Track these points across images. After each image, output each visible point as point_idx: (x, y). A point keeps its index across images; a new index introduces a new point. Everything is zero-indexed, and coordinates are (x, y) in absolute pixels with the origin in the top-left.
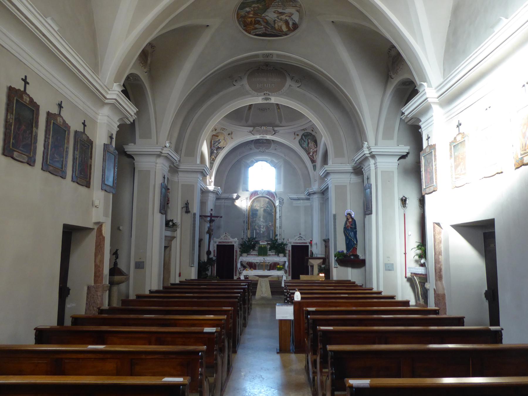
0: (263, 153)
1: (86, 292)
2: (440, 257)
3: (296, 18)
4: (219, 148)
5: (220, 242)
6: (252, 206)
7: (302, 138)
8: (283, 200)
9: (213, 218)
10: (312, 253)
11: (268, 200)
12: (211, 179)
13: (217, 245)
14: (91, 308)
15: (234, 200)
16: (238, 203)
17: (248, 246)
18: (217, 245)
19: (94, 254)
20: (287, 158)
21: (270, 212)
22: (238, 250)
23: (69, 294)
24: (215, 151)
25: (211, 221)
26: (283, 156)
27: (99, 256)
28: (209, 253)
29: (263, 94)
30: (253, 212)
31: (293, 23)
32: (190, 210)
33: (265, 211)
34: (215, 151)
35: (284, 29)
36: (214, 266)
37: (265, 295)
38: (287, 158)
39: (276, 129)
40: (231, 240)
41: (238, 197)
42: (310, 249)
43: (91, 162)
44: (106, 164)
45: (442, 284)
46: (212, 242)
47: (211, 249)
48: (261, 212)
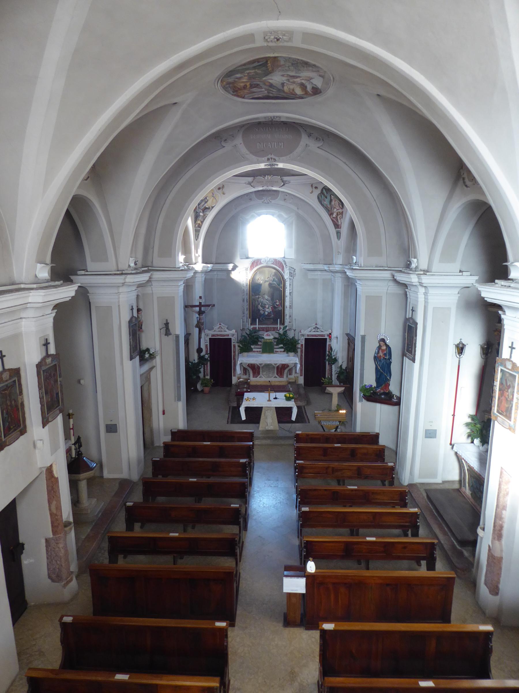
0: (267, 205)
1: (44, 544)
2: (504, 512)
3: (318, 82)
4: (205, 209)
5: (213, 335)
6: (253, 279)
7: (322, 192)
8: (294, 271)
9: (203, 309)
10: (331, 349)
11: (274, 271)
12: (197, 252)
13: (210, 339)
14: (54, 562)
15: (229, 272)
16: (234, 275)
18: (210, 339)
19: (47, 501)
20: (300, 212)
21: (278, 290)
23: (23, 549)
24: (201, 214)
26: (295, 208)
27: (54, 503)
28: (199, 350)
29: (266, 158)
30: (255, 288)
31: (313, 88)
32: (171, 331)
33: (270, 285)
34: (201, 214)
35: (299, 91)
36: (207, 364)
37: (271, 428)
38: (300, 212)
39: (285, 178)
40: (228, 332)
42: (328, 343)
43: (22, 399)
45: (501, 545)
46: (203, 335)
47: (203, 346)
48: (265, 287)
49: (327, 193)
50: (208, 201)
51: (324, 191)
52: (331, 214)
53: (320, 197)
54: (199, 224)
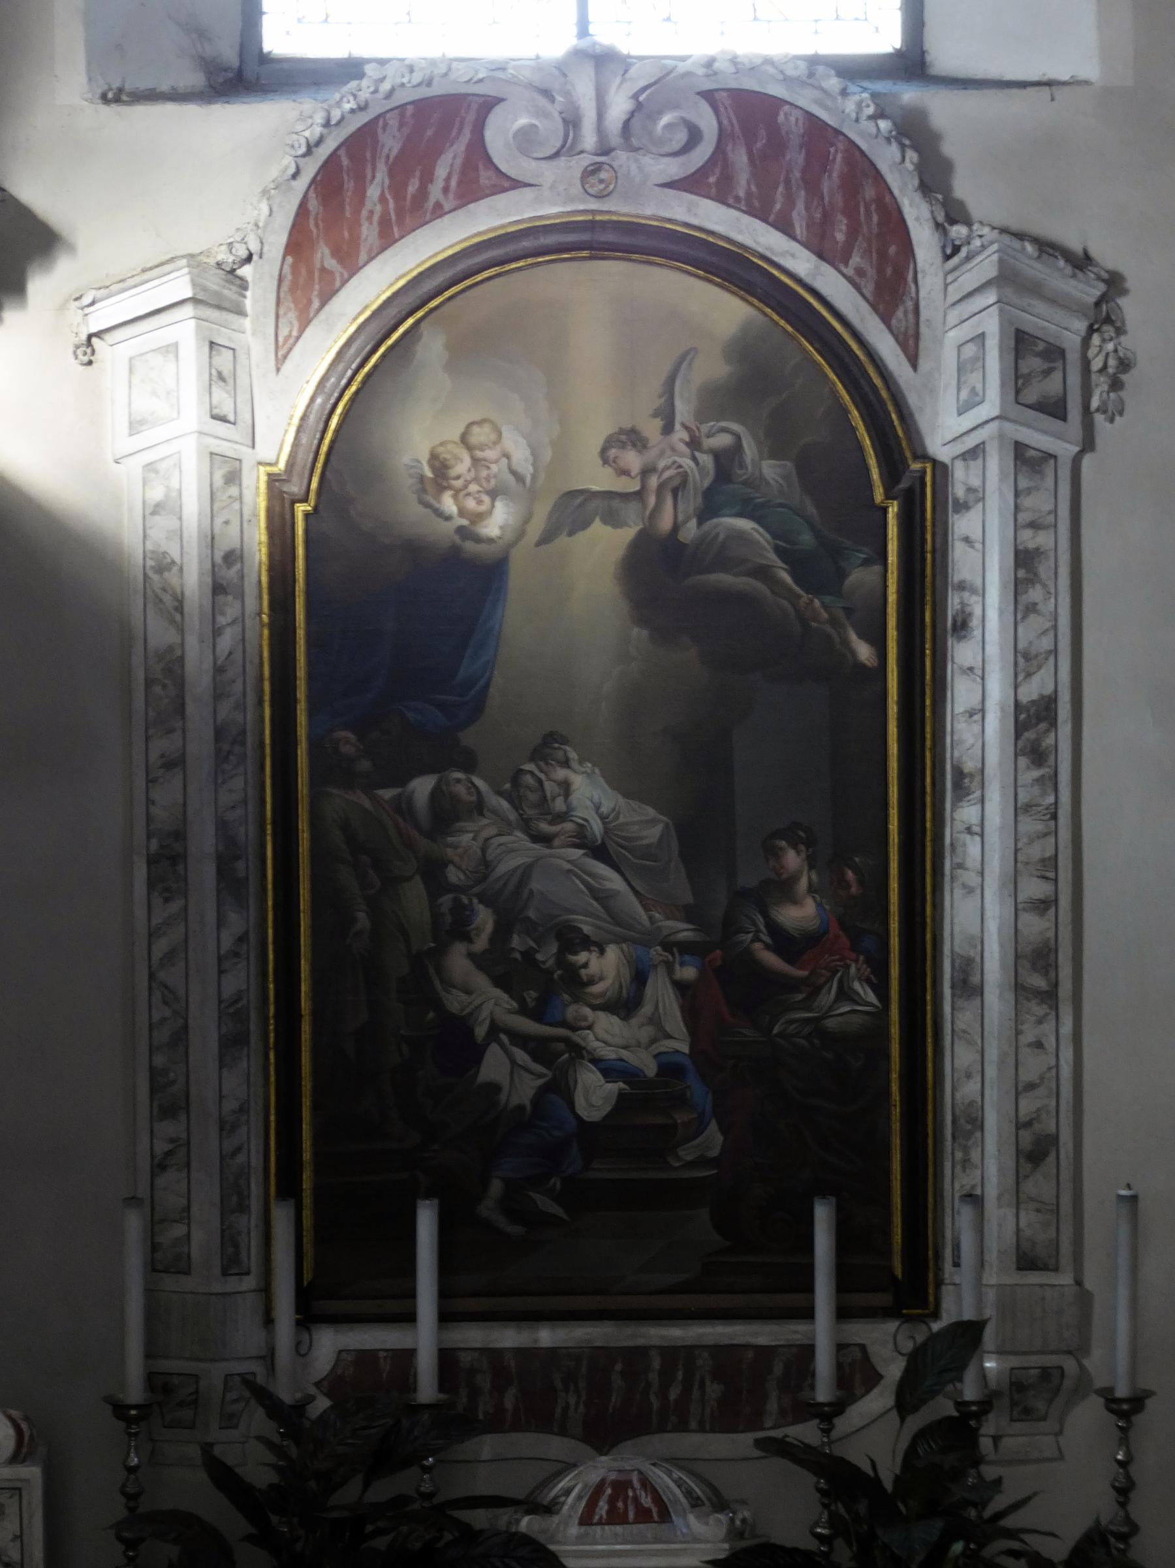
6: (344, 452)
8: (1104, 317)
11: (727, 312)
33: (660, 573)
44: (709, 1546)
48: (572, 608)
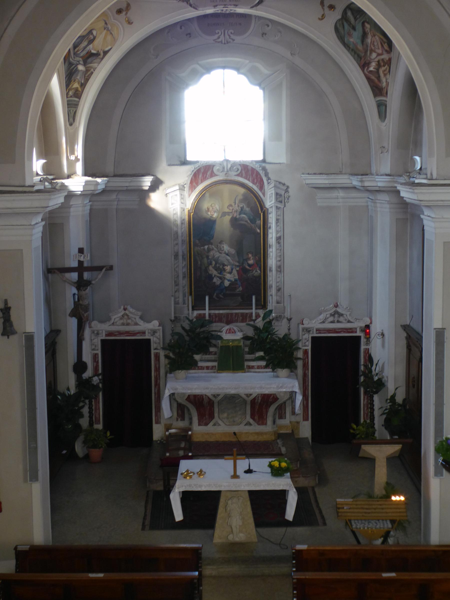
5: (110, 334)
6: (197, 208)
7: (344, 17)
8: (287, 191)
13: (102, 341)
15: (143, 195)
17: (189, 347)
18: (102, 341)
21: (251, 230)
22: (163, 361)
24: (81, 68)
25: (81, 284)
28: (80, 367)
30: (200, 228)
33: (234, 222)
34: (81, 68)
36: (97, 397)
37: (240, 537)
40: (143, 326)
41: (156, 185)
42: (363, 347)
46: (87, 332)
47: (87, 358)
48: (224, 227)
49: (356, 19)
50: (95, 38)
51: (349, 14)
52: (364, 65)
53: (341, 29)
54: (77, 90)
